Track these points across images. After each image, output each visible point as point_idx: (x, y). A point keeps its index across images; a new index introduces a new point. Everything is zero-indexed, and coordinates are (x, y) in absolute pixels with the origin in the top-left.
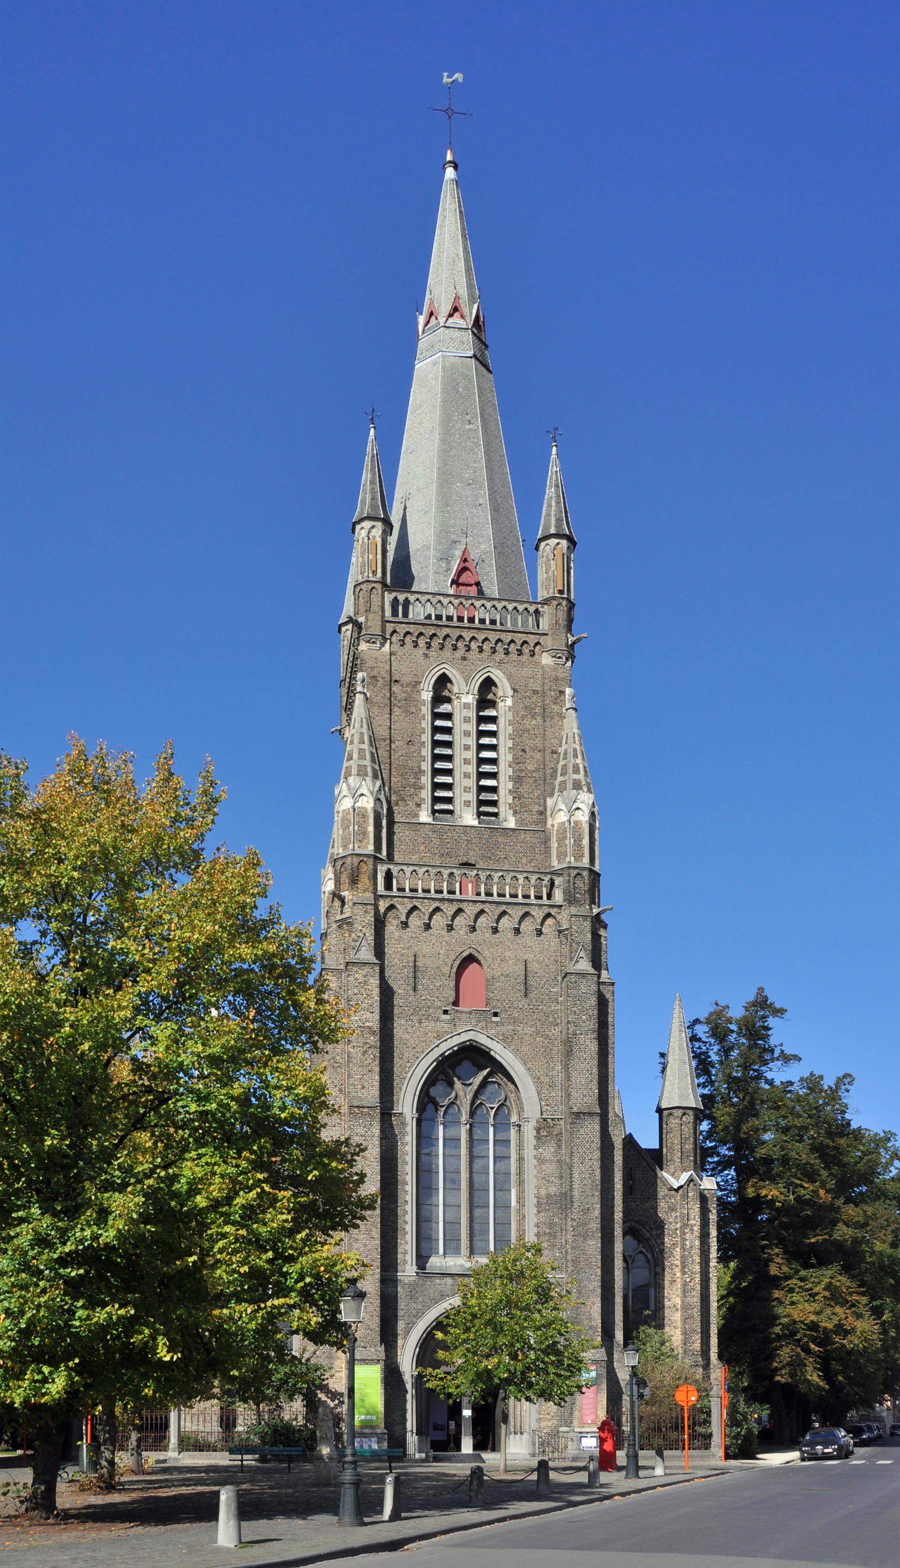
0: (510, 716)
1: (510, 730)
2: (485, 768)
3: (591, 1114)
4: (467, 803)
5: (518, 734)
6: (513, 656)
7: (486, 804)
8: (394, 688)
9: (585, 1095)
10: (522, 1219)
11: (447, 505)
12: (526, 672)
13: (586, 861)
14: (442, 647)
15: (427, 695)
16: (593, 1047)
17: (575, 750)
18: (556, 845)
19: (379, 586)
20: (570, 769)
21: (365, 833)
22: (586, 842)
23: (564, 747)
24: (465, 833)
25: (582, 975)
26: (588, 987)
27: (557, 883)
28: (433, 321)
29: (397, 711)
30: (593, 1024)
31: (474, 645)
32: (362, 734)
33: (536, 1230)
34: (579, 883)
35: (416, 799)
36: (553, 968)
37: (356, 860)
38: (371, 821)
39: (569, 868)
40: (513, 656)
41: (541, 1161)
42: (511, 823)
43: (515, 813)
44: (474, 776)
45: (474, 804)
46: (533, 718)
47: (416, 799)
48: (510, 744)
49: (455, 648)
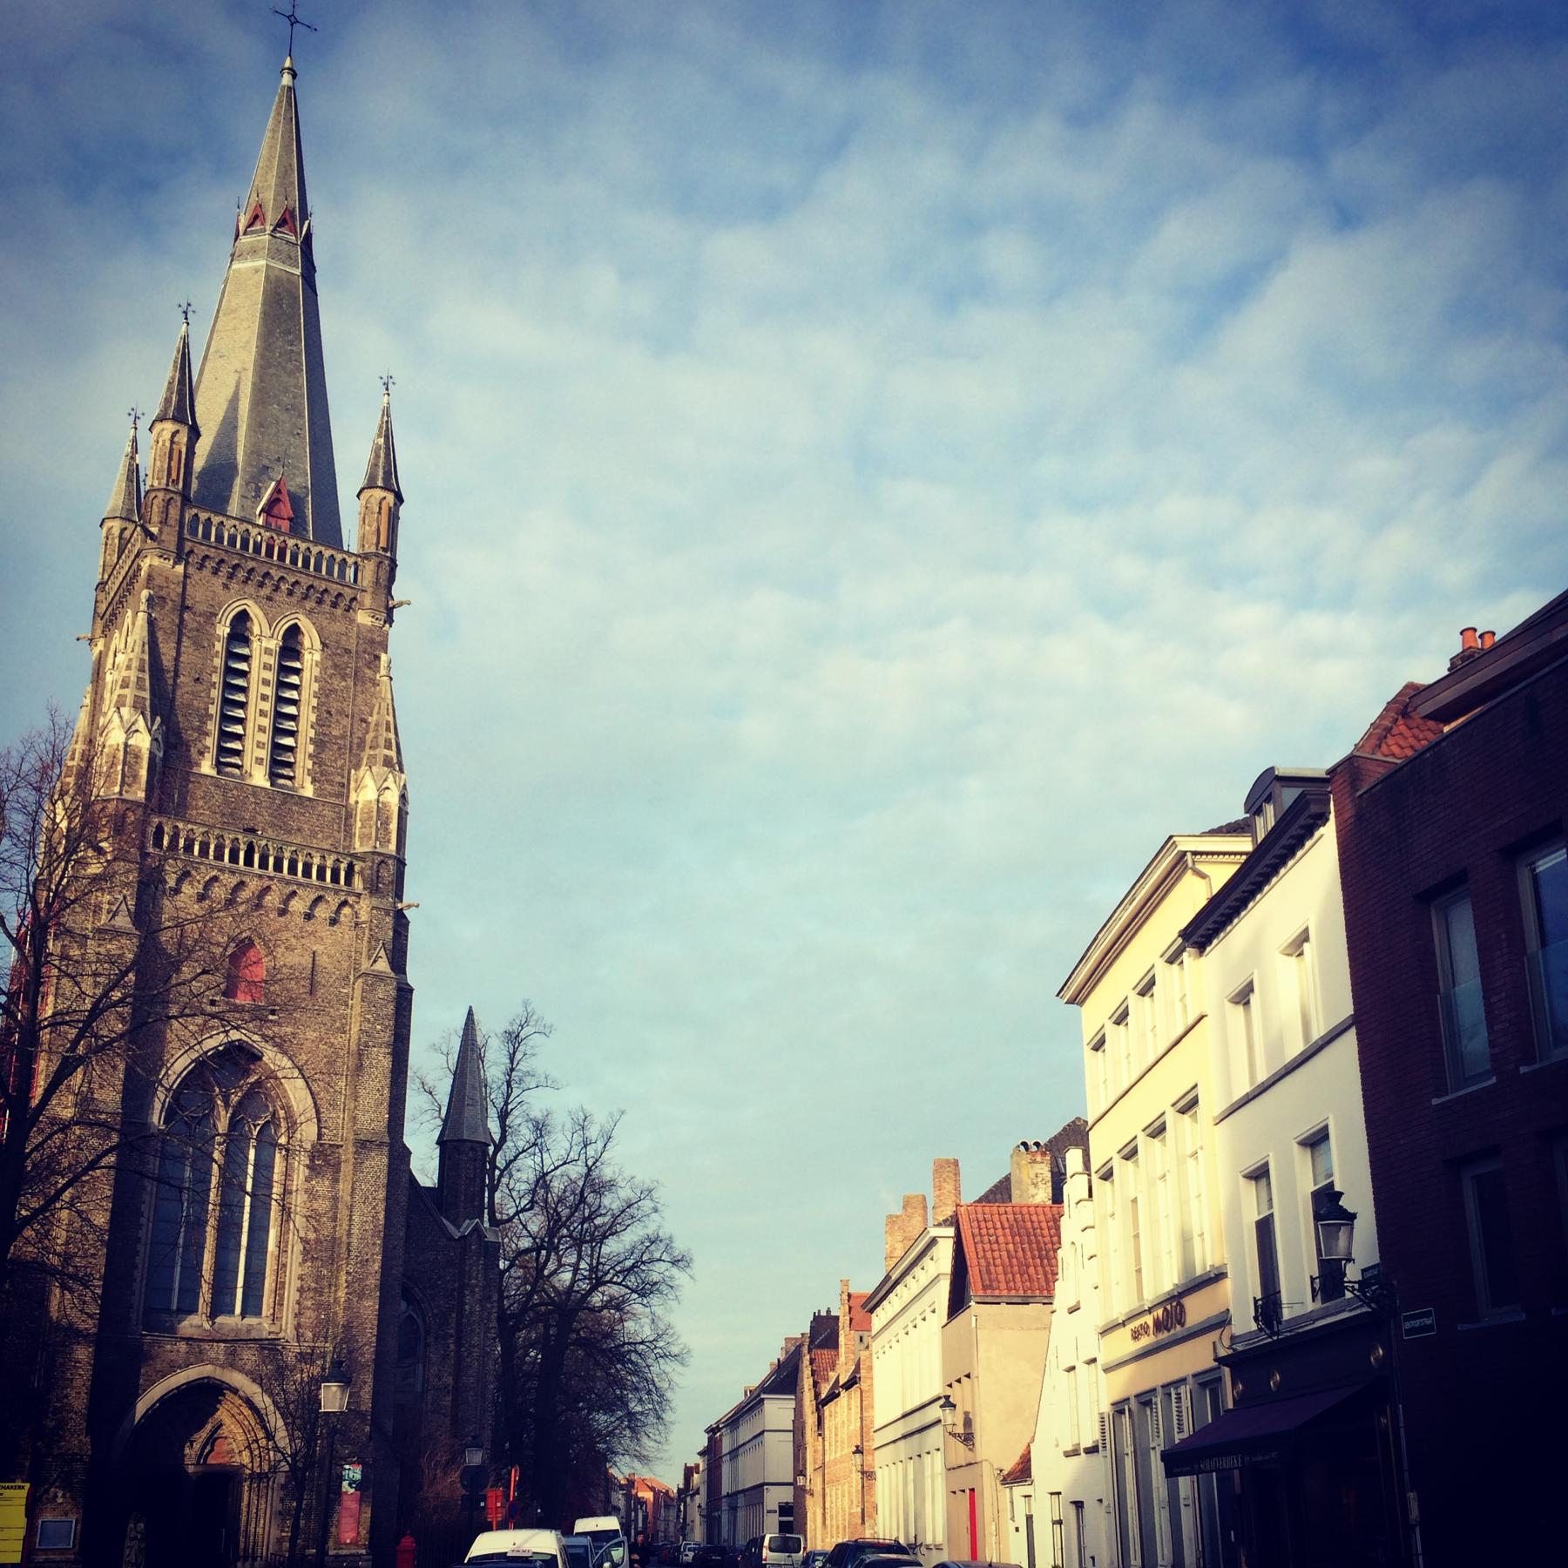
0: (316, 672)
1: (315, 686)
2: (281, 724)
3: (382, 1143)
4: (259, 761)
5: (325, 693)
6: (326, 607)
7: (279, 762)
8: (185, 616)
9: (373, 1118)
10: (281, 1267)
11: (261, 425)
12: (338, 627)
13: (392, 847)
14: (290, 593)
15: (223, 630)
16: (386, 1062)
17: (388, 723)
18: (359, 824)
19: (178, 499)
20: (382, 742)
21: (135, 777)
22: (393, 826)
23: (375, 716)
24: (254, 794)
25: (379, 977)
26: (386, 992)
27: (357, 868)
28: (257, 227)
29: (186, 642)
30: (387, 1037)
31: (284, 587)
32: (142, 660)
33: (299, 1283)
34: (384, 873)
35: (199, 746)
36: (345, 965)
37: (122, 807)
38: (145, 764)
39: (373, 853)
40: (326, 607)
41: (312, 1195)
42: (308, 791)
43: (314, 781)
44: (269, 730)
45: (267, 762)
46: (344, 678)
47: (199, 746)
48: (314, 702)
49: (261, 585)
